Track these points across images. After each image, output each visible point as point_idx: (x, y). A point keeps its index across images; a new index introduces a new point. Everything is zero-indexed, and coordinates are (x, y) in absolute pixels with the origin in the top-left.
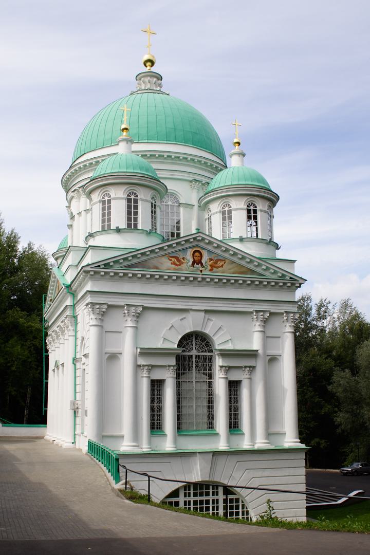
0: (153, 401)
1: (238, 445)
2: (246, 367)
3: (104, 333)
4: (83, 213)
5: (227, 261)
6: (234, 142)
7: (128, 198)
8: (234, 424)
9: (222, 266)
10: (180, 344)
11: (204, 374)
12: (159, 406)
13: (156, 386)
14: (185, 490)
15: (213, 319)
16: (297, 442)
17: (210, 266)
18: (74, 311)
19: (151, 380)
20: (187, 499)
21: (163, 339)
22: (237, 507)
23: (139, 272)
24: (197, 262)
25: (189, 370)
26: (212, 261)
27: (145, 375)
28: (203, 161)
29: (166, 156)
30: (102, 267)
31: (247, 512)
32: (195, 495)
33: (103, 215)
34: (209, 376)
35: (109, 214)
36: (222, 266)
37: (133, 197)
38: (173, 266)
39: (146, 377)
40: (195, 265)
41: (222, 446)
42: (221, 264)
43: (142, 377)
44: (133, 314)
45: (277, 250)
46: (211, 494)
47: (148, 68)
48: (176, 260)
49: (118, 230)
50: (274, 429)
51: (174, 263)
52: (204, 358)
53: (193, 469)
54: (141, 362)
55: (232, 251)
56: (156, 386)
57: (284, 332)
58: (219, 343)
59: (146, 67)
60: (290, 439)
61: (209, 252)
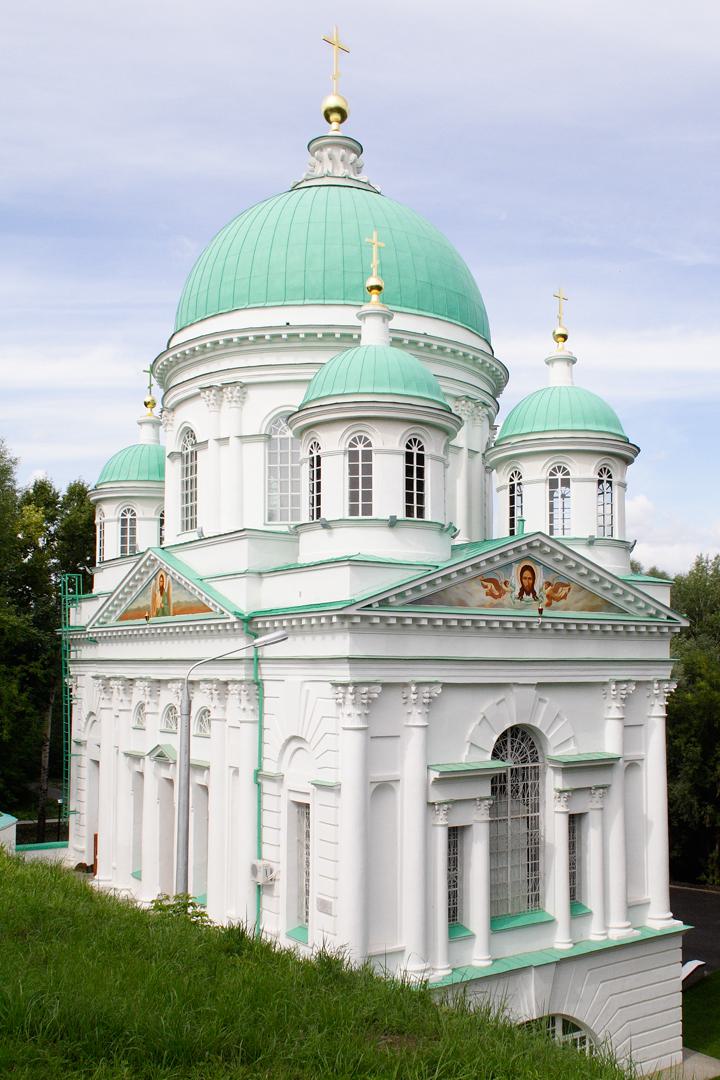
1: (582, 935)
2: (597, 788)
3: (374, 739)
4: (234, 441)
5: (573, 586)
6: (557, 333)
9: (565, 597)
13: (455, 834)
15: (547, 699)
16: (669, 919)
17: (548, 596)
18: (256, 672)
21: (469, 744)
23: (439, 613)
24: (527, 589)
27: (441, 823)
28: (461, 351)
29: (422, 345)
30: (374, 606)
33: (354, 483)
35: (368, 483)
36: (565, 597)
38: (489, 599)
39: (442, 826)
40: (525, 596)
41: (560, 942)
42: (564, 592)
43: (435, 825)
44: (425, 701)
47: (335, 125)
49: (393, 523)
50: (635, 898)
51: (490, 594)
53: (522, 996)
54: (437, 796)
55: (586, 568)
57: (650, 717)
59: (330, 123)
60: (659, 918)
61: (546, 568)
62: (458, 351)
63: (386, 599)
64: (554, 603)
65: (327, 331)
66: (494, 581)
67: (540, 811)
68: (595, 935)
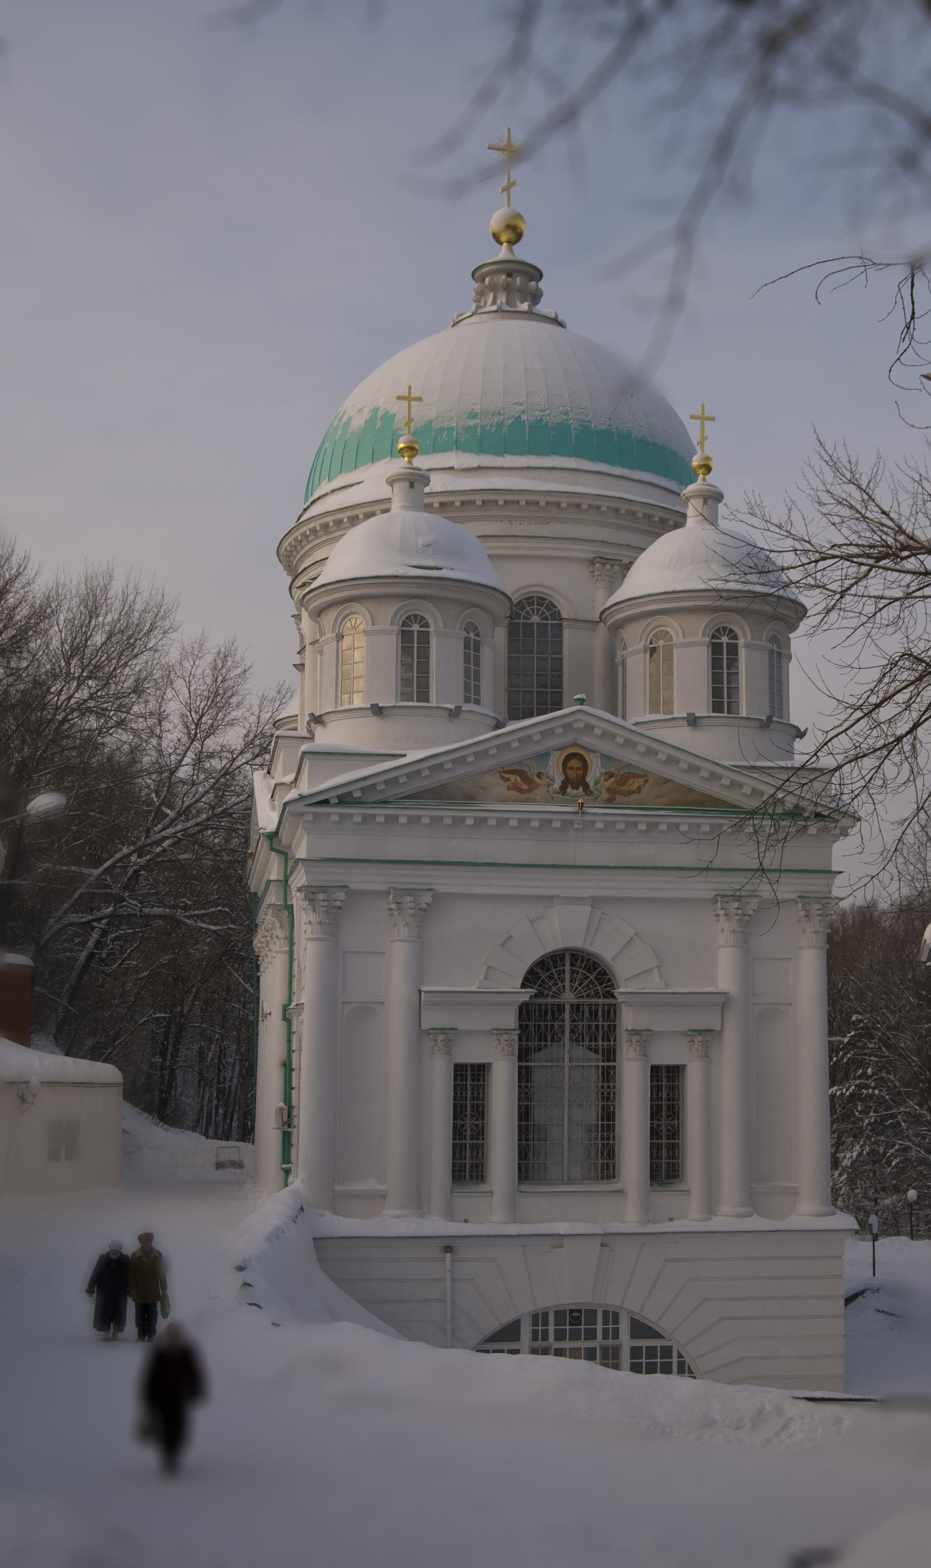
0: (657, 1113)
7: (713, 643)
8: (665, 1166)
9: (639, 789)
10: (530, 979)
11: (590, 1049)
12: (477, 1126)
17: (608, 790)
19: (656, 1070)
20: (610, 1342)
25: (553, 1040)
26: (613, 779)
34: (603, 1055)
36: (639, 789)
37: (725, 640)
40: (569, 790)
42: (636, 785)
45: (798, 739)
46: (599, 1334)
48: (519, 779)
52: (540, 1011)
54: (430, 1020)
56: (470, 1081)
58: (631, 975)
61: (606, 758)
62: (653, 516)
64: (619, 798)
65: (552, 499)
66: (522, 774)
68: (718, 1223)
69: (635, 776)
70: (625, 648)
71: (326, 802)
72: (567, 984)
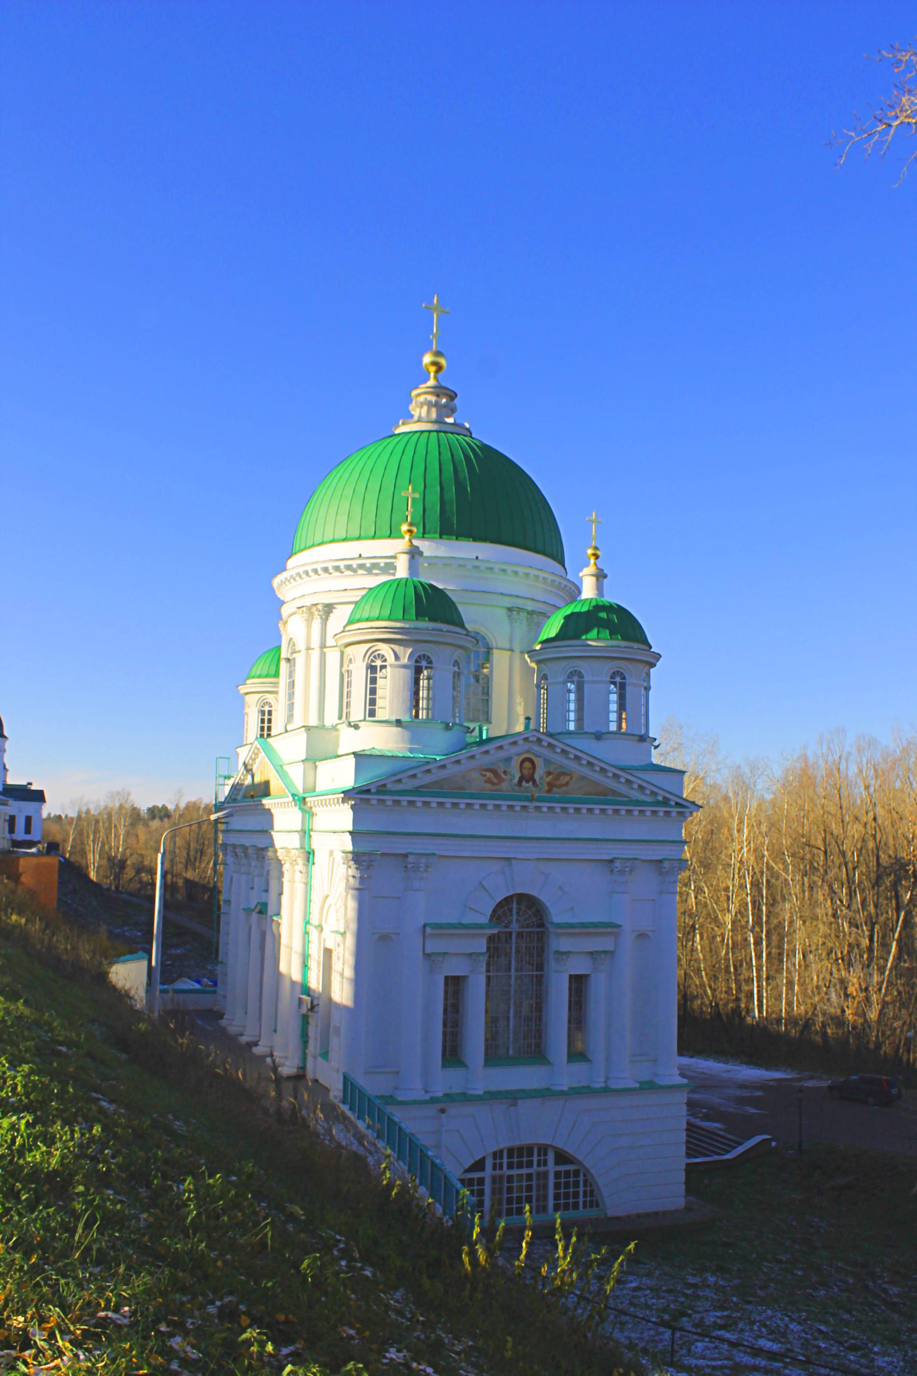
13: (455, 984)
14: (495, 1158)
17: (548, 784)
20: (542, 1169)
22: (576, 1184)
31: (592, 1191)
32: (510, 1166)
36: (567, 784)
40: (524, 783)
41: (567, 1075)
48: (492, 775)
56: (455, 984)
61: (547, 762)
63: (384, 785)
64: (555, 789)
67: (545, 969)
69: (565, 774)
70: (779, 1021)
71: (368, 791)
72: (515, 917)
